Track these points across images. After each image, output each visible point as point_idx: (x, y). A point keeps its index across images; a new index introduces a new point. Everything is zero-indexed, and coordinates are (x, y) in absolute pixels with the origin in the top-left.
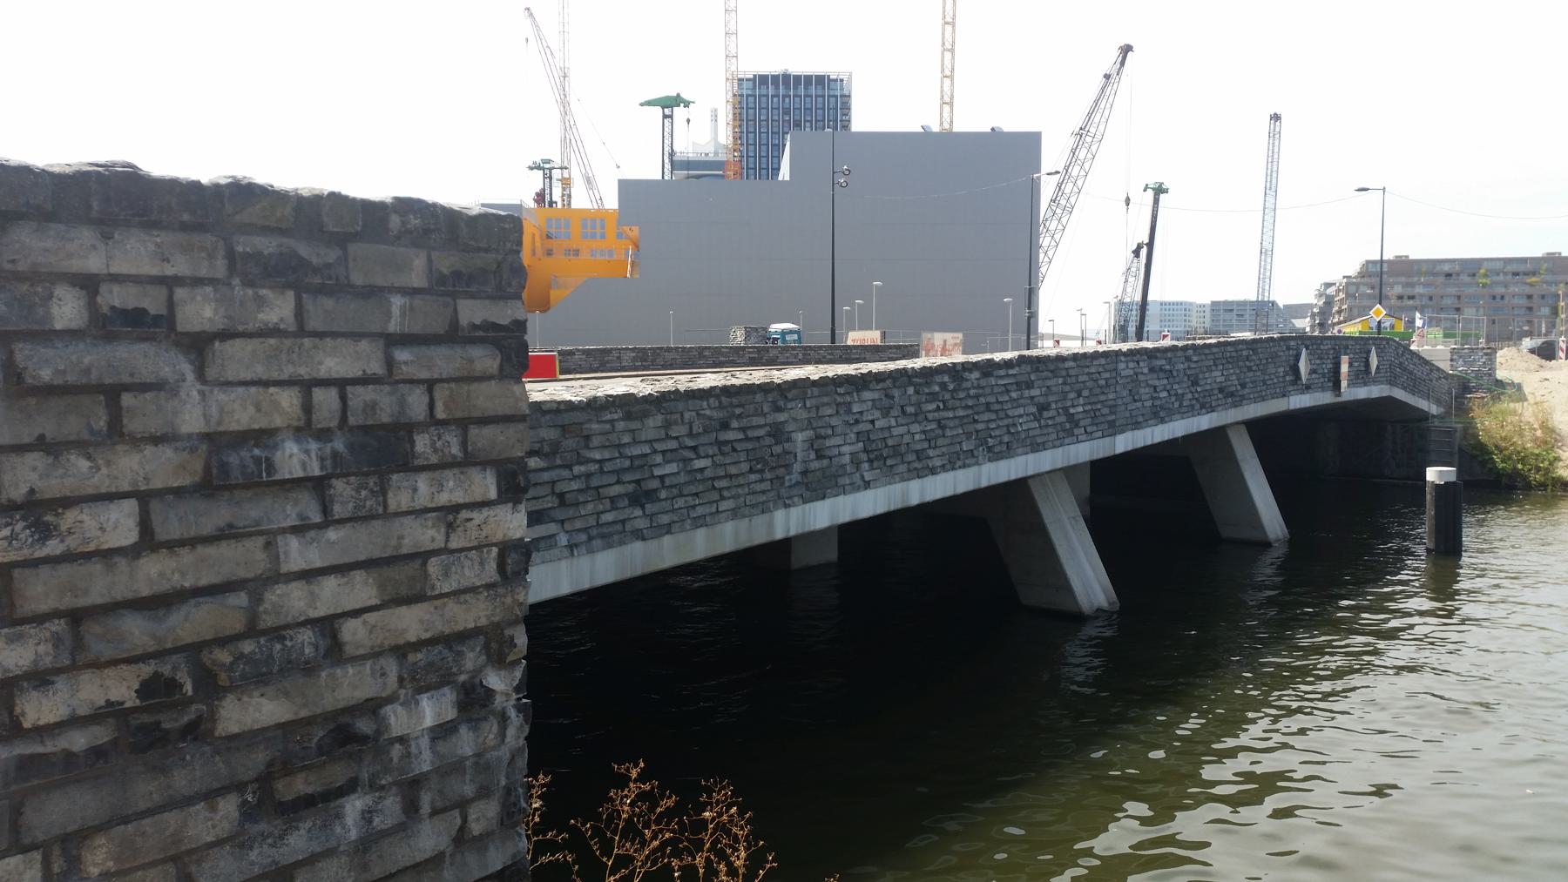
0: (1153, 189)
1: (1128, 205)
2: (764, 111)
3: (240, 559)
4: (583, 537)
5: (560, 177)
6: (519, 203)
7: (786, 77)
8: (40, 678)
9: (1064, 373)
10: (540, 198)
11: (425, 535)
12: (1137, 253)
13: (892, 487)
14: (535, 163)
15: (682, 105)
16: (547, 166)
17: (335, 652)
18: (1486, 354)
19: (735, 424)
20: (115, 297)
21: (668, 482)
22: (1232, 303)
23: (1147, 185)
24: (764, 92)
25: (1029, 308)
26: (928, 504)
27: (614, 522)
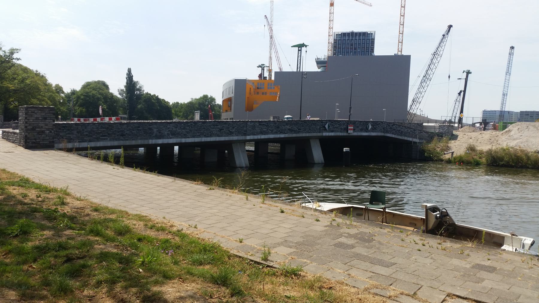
0: (466, 72)
1: (449, 78)
2: (344, 45)
3: (38, 123)
4: (112, 139)
5: (268, 69)
6: (246, 79)
7: (352, 33)
8: (28, 126)
9: (228, 124)
10: (260, 76)
11: (48, 123)
12: (459, 94)
13: (178, 139)
14: (259, 65)
15: (305, 46)
16: (263, 66)
17: (42, 128)
18: (447, 127)
19: (141, 127)
20: (32, 111)
21: (127, 134)
22: (529, 112)
23: (464, 71)
24: (344, 38)
25: (350, 112)
26: (187, 143)
27: (118, 138)
